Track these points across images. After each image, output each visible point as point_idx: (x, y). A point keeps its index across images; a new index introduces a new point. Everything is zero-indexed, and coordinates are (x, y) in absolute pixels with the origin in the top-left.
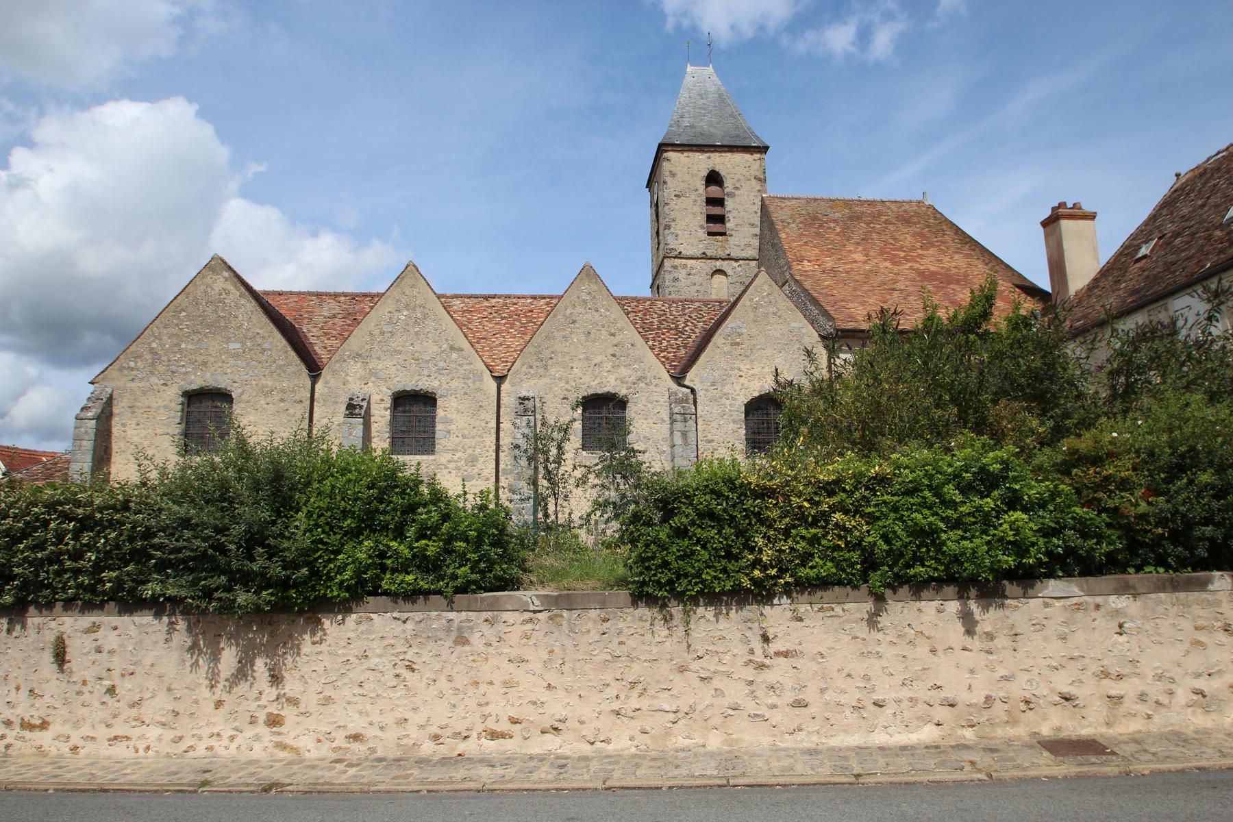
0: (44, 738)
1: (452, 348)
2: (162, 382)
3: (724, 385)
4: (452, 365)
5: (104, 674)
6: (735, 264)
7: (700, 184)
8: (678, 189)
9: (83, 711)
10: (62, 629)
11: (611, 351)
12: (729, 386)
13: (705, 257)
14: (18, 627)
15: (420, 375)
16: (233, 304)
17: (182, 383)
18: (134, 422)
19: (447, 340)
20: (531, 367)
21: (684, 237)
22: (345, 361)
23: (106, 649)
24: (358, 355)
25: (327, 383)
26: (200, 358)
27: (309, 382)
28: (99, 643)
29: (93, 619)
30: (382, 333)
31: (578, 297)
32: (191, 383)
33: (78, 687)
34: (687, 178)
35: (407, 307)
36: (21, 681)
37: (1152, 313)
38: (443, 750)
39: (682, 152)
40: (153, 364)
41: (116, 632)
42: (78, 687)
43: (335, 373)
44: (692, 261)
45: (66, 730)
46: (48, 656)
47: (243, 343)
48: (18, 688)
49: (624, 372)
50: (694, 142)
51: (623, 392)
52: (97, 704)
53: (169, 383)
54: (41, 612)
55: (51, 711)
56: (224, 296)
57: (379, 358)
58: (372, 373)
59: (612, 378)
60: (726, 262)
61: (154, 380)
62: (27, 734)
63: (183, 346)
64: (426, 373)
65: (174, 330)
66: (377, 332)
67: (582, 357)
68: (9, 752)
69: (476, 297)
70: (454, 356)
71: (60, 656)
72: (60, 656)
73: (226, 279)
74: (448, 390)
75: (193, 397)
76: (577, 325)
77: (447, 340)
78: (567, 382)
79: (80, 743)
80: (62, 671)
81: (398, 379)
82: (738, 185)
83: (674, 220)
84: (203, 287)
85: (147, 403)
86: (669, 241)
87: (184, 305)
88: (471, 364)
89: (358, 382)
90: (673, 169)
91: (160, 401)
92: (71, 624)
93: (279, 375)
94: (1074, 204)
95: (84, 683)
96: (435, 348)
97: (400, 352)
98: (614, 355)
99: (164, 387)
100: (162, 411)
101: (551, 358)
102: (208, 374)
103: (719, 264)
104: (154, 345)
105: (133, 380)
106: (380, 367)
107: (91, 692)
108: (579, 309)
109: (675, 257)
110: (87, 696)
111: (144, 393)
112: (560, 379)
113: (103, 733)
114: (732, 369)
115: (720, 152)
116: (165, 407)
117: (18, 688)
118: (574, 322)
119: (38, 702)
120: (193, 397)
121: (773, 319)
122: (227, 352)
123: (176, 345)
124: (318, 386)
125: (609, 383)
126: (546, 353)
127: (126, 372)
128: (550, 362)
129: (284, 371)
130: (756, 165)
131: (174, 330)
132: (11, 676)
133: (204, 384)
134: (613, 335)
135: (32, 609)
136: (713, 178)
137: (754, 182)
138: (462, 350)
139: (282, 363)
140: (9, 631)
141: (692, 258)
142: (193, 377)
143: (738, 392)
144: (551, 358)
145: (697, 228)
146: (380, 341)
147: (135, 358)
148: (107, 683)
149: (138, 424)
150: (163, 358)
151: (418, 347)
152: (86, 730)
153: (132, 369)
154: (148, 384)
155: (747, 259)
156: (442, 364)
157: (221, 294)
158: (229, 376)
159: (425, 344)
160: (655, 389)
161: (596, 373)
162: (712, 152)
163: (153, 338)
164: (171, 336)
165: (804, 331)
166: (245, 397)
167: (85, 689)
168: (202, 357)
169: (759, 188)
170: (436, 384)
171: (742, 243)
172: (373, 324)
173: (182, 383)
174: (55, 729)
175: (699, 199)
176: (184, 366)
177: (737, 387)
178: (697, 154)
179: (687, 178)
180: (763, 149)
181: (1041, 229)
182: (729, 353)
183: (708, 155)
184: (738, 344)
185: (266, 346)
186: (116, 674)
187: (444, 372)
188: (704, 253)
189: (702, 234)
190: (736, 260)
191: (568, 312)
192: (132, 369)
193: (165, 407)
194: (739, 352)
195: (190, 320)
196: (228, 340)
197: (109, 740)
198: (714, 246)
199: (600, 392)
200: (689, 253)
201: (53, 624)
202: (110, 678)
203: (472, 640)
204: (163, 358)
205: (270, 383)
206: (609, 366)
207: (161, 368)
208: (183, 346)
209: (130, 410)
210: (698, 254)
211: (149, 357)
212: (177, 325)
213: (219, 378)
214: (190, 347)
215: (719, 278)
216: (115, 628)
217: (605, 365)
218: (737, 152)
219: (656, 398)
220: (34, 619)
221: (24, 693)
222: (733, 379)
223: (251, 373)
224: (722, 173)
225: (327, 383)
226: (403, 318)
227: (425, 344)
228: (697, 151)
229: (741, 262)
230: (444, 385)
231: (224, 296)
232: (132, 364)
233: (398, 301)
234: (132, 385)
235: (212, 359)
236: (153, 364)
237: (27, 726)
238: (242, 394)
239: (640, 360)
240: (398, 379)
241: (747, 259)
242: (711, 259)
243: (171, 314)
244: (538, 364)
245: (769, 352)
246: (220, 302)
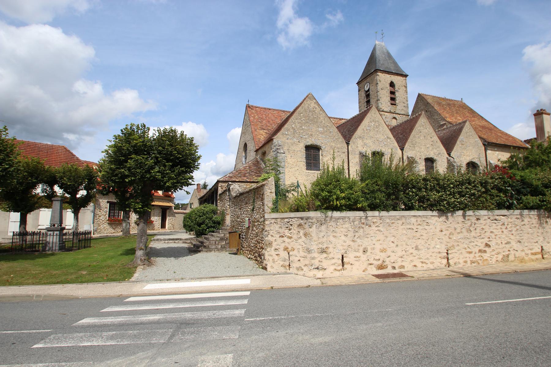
1: (388, 138)
2: (298, 141)
3: (460, 158)
6: (399, 116)
11: (431, 143)
12: (462, 158)
13: (390, 112)
16: (318, 113)
20: (410, 147)
21: (384, 104)
24: (360, 137)
25: (352, 146)
27: (346, 145)
30: (367, 130)
32: (308, 142)
34: (384, 83)
35: (373, 121)
38: (395, 271)
40: (294, 133)
43: (354, 143)
44: (387, 113)
47: (323, 129)
49: (435, 151)
50: (386, 70)
51: (435, 158)
57: (367, 139)
59: (432, 153)
60: (397, 115)
61: (295, 140)
63: (303, 127)
65: (299, 121)
66: (365, 129)
69: (337, 118)
70: (389, 140)
73: (315, 103)
74: (388, 153)
76: (422, 133)
78: (420, 153)
81: (373, 147)
83: (381, 98)
84: (307, 105)
90: (380, 79)
91: (298, 148)
98: (432, 145)
100: (299, 152)
102: (313, 139)
104: (293, 126)
108: (422, 128)
111: (292, 144)
112: (418, 152)
114: (462, 152)
115: (394, 75)
116: (300, 151)
118: (421, 132)
122: (319, 131)
124: (349, 147)
125: (431, 155)
126: (414, 142)
128: (415, 145)
130: (404, 82)
131: (299, 121)
134: (431, 138)
136: (392, 84)
137: (404, 87)
139: (337, 137)
141: (387, 112)
147: (287, 130)
151: (378, 136)
153: (287, 135)
155: (403, 115)
157: (313, 109)
158: (320, 141)
159: (380, 135)
163: (292, 123)
164: (299, 123)
165: (479, 142)
166: (326, 149)
168: (311, 133)
169: (405, 90)
171: (401, 109)
173: (305, 142)
176: (305, 135)
177: (464, 159)
178: (387, 75)
179: (384, 83)
180: (406, 76)
181: (533, 116)
182: (461, 147)
183: (390, 75)
184: (463, 144)
185: (331, 130)
187: (386, 146)
188: (390, 111)
189: (389, 104)
190: (399, 114)
191: (419, 129)
192: (287, 135)
193: (300, 151)
195: (305, 118)
196: (318, 127)
198: (392, 108)
199: (429, 157)
203: (525, 220)
205: (334, 145)
206: (431, 148)
208: (303, 127)
209: (288, 151)
210: (388, 111)
212: (300, 119)
213: (317, 141)
214: (305, 128)
217: (430, 148)
218: (399, 76)
219: (444, 160)
222: (462, 156)
223: (327, 140)
224: (395, 83)
225: (352, 146)
227: (380, 135)
228: (387, 74)
229: (401, 115)
230: (387, 151)
231: (314, 109)
232: (287, 133)
233: (371, 118)
234: (288, 141)
235: (314, 134)
236: (294, 133)
238: (325, 148)
239: (439, 147)
240: (373, 147)
241: (403, 115)
242: (392, 113)
244: (412, 146)
245: (471, 148)
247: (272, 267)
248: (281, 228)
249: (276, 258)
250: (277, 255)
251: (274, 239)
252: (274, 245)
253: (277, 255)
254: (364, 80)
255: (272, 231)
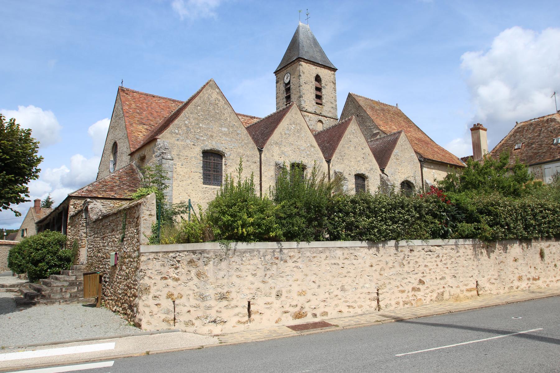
0: (539, 283)
1: (311, 146)
2: (192, 143)
4: (312, 154)
5: (553, 261)
6: (326, 119)
7: (313, 79)
8: (306, 80)
9: (549, 273)
10: (541, 246)
11: (362, 156)
12: (396, 176)
13: (315, 113)
14: (530, 246)
15: (300, 156)
17: (202, 145)
18: (180, 164)
19: (309, 141)
20: (338, 159)
22: (272, 145)
23: (552, 253)
24: (277, 143)
26: (209, 133)
28: (550, 251)
29: (549, 243)
30: (285, 134)
31: (351, 131)
33: (547, 265)
34: (309, 76)
35: (294, 123)
36: (531, 265)
37: (534, 168)
39: (307, 63)
41: (555, 247)
42: (547, 265)
43: (268, 150)
45: (545, 279)
46: (538, 256)
48: (531, 267)
52: (552, 270)
53: (196, 144)
54: (535, 241)
55: (540, 274)
56: (217, 102)
58: (283, 153)
59: (363, 167)
61: (188, 141)
62: (534, 282)
63: (201, 125)
64: (303, 156)
65: (195, 116)
66: (283, 133)
67: (354, 157)
68: (530, 289)
69: (247, 116)
70: (312, 149)
71: (542, 255)
72: (542, 255)
75: (207, 154)
77: (309, 141)
78: (350, 167)
79: (549, 283)
80: (542, 260)
81: (293, 157)
82: (326, 84)
83: (304, 94)
85: (186, 154)
86: (302, 103)
87: (199, 103)
88: (318, 154)
89: (278, 156)
91: (192, 153)
92: (543, 244)
93: (245, 148)
94: (478, 124)
95: (549, 264)
96: (305, 145)
97: (293, 145)
98: (363, 158)
99: (194, 147)
100: (194, 159)
101: (344, 156)
102: (214, 143)
103: (320, 118)
104: (186, 122)
105: (178, 140)
106: (285, 150)
107: (550, 267)
108: (352, 136)
109: (305, 111)
110: (549, 268)
111: (184, 148)
112: (348, 166)
113: (554, 279)
115: (320, 67)
116: (195, 157)
117: (531, 267)
118: (350, 141)
119: (537, 271)
120: (207, 154)
121: (406, 151)
123: (197, 124)
124: (262, 155)
125: (362, 170)
126: (343, 153)
127: (174, 135)
129: (248, 146)
130: (332, 77)
131: (195, 116)
132: (528, 263)
133: (212, 148)
135: (533, 241)
136: (318, 79)
137: (332, 84)
138: (315, 147)
139: (246, 142)
140: (527, 248)
141: (311, 113)
142: (207, 143)
143: (398, 179)
144: (344, 156)
145: (313, 100)
146: (285, 138)
147: (178, 128)
148: (554, 263)
149: (182, 165)
150: (192, 130)
151: (299, 143)
152: (550, 279)
153: (177, 134)
154: (185, 143)
155: (330, 118)
156: (308, 152)
158: (224, 145)
159: (301, 142)
160: (376, 174)
161: (358, 165)
162: (318, 66)
164: (195, 119)
166: (231, 157)
167: (549, 266)
168: (211, 133)
169: (333, 87)
170: (306, 161)
171: (328, 110)
172: (282, 129)
173: (202, 145)
174: (542, 279)
175: (313, 86)
176: (202, 136)
178: (312, 66)
179: (309, 76)
180: (335, 70)
183: (316, 67)
185: (238, 132)
186: (556, 260)
187: (309, 156)
188: (315, 112)
190: (326, 117)
192: (177, 134)
193: (195, 157)
194: (398, 162)
196: (221, 126)
197: (556, 281)
200: (309, 110)
201: (539, 245)
202: (554, 262)
204: (192, 130)
205: (242, 151)
206: (362, 162)
207: (191, 136)
210: (313, 112)
211: (185, 128)
212: (197, 113)
213: (219, 145)
214: (204, 126)
215: (320, 124)
216: (554, 246)
218: (326, 69)
220: (534, 243)
221: (533, 268)
223: (233, 145)
225: (265, 155)
226: (293, 128)
228: (312, 64)
229: (328, 118)
231: (217, 102)
233: (290, 120)
234: (178, 143)
235: (215, 135)
237: (534, 279)
238: (230, 155)
240: (293, 157)
241: (330, 118)
243: (193, 107)
244: (340, 158)
245: (406, 164)
246: (216, 105)
247: (149, 323)
248: (164, 265)
249: (155, 309)
250: (156, 305)
251: (153, 281)
252: (153, 291)
253: (156, 305)
254: (283, 69)
255: (150, 271)
